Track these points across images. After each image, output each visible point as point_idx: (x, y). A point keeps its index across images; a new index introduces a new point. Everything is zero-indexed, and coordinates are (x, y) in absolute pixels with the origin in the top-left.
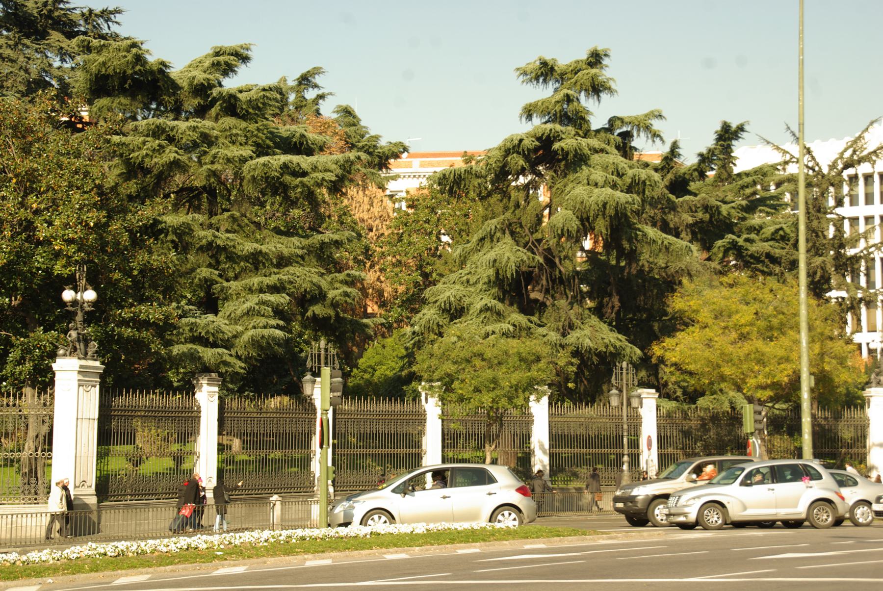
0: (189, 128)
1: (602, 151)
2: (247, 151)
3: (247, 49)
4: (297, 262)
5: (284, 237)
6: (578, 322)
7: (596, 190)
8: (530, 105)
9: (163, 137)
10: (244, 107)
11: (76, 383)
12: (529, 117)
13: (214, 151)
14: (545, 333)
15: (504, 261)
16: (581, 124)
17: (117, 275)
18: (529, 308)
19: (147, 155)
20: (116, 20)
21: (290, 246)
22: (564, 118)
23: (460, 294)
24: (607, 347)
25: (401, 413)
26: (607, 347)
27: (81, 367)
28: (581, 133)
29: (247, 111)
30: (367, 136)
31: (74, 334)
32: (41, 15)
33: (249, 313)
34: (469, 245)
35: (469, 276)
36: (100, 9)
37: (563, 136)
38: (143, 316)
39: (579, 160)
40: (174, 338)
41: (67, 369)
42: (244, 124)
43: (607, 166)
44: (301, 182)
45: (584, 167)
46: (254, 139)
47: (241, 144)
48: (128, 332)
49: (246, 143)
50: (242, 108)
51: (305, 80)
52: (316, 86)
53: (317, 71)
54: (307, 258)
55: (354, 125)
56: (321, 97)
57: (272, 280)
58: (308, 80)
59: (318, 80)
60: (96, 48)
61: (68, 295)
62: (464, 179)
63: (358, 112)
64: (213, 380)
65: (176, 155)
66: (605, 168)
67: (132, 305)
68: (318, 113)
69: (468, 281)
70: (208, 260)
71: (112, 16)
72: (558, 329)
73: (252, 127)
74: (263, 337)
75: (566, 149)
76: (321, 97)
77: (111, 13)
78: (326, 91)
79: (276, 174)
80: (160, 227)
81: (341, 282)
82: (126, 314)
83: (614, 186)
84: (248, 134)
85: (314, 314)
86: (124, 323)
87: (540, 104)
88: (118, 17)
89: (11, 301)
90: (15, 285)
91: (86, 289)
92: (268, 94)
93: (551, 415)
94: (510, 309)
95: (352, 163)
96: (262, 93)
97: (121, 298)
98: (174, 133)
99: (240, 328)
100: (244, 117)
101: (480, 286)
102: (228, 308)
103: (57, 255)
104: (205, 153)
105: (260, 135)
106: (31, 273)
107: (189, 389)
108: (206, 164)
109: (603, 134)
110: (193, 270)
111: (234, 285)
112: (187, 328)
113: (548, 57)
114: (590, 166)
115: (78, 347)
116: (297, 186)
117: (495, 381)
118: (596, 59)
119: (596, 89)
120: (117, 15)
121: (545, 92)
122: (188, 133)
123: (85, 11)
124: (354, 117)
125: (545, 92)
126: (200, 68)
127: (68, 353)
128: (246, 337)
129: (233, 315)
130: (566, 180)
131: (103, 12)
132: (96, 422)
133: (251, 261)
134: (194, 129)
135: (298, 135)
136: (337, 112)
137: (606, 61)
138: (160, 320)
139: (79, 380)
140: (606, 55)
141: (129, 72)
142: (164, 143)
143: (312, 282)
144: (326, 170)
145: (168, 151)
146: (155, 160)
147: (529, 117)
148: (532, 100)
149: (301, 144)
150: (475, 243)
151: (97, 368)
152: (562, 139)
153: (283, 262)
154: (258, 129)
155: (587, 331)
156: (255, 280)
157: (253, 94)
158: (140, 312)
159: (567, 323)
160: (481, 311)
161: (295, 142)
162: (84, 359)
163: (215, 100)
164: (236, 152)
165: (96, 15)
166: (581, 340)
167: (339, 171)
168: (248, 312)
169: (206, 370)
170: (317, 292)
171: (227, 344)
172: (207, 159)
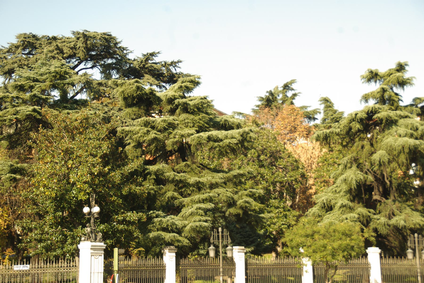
0: (162, 121)
1: (406, 117)
2: (193, 131)
3: (199, 78)
4: (221, 186)
5: (215, 173)
6: (396, 212)
7: (400, 139)
8: (366, 95)
9: (149, 126)
10: (192, 108)
11: (90, 255)
12: (366, 101)
13: (176, 131)
14: (379, 217)
15: (350, 179)
16: (393, 103)
17: (114, 198)
18: (371, 204)
19: (141, 136)
20: (179, 66)
21: (218, 178)
22: (382, 101)
23: (330, 198)
24: (415, 225)
25: (288, 264)
26: (415, 225)
27: (92, 246)
28: (393, 108)
29: (194, 110)
30: (338, 112)
31: (89, 229)
32: (140, 68)
33: (192, 214)
34: (338, 171)
35: (336, 188)
36: (170, 61)
37: (380, 110)
38: (128, 219)
39: (390, 123)
40: (152, 228)
41: (85, 247)
42: (192, 117)
43: (408, 125)
44: (218, 145)
45: (393, 127)
46: (198, 124)
47: (190, 127)
48: (121, 227)
49: (193, 126)
50: (191, 109)
51: (286, 87)
52: (293, 89)
53: (293, 82)
54: (228, 183)
55: (330, 107)
56: (295, 95)
57: (206, 196)
58: (288, 86)
59: (293, 86)
60: (120, 84)
61: (86, 210)
62: (329, 137)
63: (332, 101)
64: (172, 249)
65: (155, 135)
66: (407, 126)
67: (123, 213)
68: (292, 103)
69: (336, 191)
70: (173, 187)
71: (177, 64)
72: (386, 216)
73: (197, 118)
74: (197, 226)
75: (381, 118)
76: (295, 95)
77: (176, 63)
78: (297, 92)
79: (204, 141)
80: (146, 172)
81: (247, 195)
82: (120, 218)
83: (411, 136)
84: (194, 122)
85: (230, 213)
86: (119, 222)
87: (370, 94)
88: (180, 65)
89: (63, 214)
90: (64, 206)
91: (95, 206)
92: (203, 101)
93: (381, 264)
94: (357, 205)
95: (248, 133)
96: (200, 101)
97: (117, 209)
98: (154, 124)
99: (186, 222)
100: (192, 113)
101: (342, 193)
102: (185, 211)
103: (80, 190)
104: (171, 133)
105: (200, 121)
106: (71, 199)
107: (160, 255)
108: (171, 138)
109: (409, 108)
110: (165, 193)
111: (186, 200)
112: (158, 223)
113: (373, 69)
114: (398, 126)
115: (91, 236)
116: (216, 147)
117: (325, 247)
118: (401, 68)
119: (402, 83)
120: (179, 63)
121: (375, 87)
122: (161, 123)
123: (163, 63)
124: (330, 103)
125: (375, 87)
126: (173, 90)
127: (86, 239)
128: (188, 228)
129: (184, 215)
130: (384, 134)
131: (172, 63)
132: (102, 274)
133: (196, 186)
134: (164, 121)
135: (223, 120)
136: (321, 101)
137: (407, 68)
138: (136, 220)
139: (91, 253)
140: (406, 65)
141: (135, 95)
142: (150, 129)
143: (227, 196)
144: (233, 138)
145: (151, 133)
146: (145, 138)
147: (366, 101)
148: (367, 92)
149: (226, 125)
150: (341, 170)
151: (102, 246)
152: (379, 112)
153: (212, 186)
154: (200, 119)
155: (403, 216)
156: (197, 197)
157: (196, 102)
158: (127, 216)
159: (391, 213)
160: (340, 207)
161: (222, 124)
162: (94, 242)
163: (177, 106)
164: (187, 131)
165: (168, 65)
166: (398, 222)
167: (240, 138)
168: (192, 213)
169: (169, 244)
170: (232, 201)
171: (179, 232)
172: (172, 136)
